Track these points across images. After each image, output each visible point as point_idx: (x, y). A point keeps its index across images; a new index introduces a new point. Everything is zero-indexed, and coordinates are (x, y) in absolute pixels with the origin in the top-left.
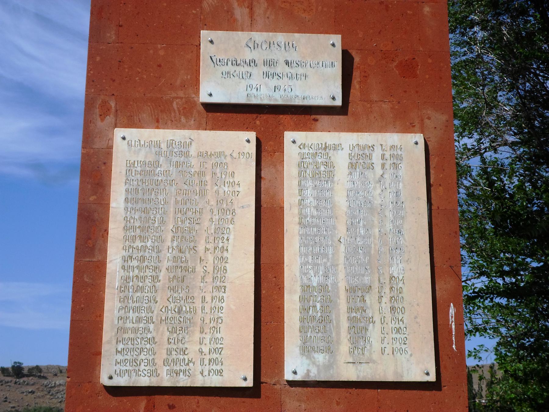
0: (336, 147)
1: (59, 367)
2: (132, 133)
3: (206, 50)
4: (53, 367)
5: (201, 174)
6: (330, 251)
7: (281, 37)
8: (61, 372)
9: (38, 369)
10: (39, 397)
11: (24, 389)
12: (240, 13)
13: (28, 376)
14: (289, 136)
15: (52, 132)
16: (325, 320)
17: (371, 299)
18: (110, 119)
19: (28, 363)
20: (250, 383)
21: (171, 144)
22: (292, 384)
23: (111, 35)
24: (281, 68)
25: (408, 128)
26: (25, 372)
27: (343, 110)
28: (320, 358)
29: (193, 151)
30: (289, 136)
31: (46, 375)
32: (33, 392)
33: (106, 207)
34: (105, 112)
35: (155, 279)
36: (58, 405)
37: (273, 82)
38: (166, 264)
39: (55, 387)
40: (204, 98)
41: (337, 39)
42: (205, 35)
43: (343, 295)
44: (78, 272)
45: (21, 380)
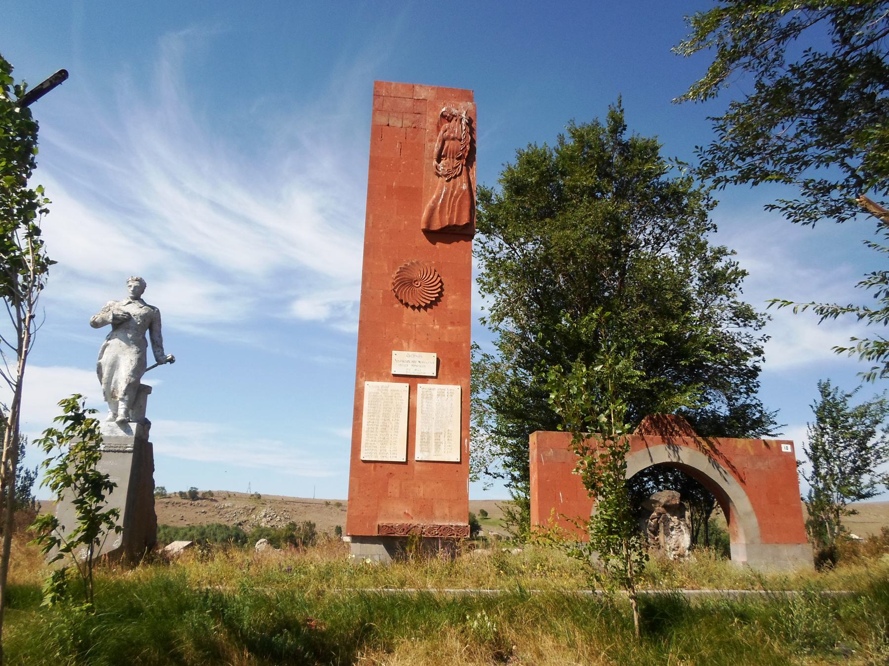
0: (433, 389)
1: (228, 492)
2: (370, 383)
3: (394, 357)
4: (223, 492)
5: (391, 396)
6: (661, 245)
7: (417, 354)
8: (229, 496)
9: (211, 493)
10: (210, 517)
11: (198, 510)
12: (405, 344)
13: (201, 499)
14: (419, 385)
15: (219, 297)
16: (428, 442)
17: (442, 436)
18: (364, 378)
19: (202, 488)
20: (405, 460)
21: (382, 387)
22: (417, 461)
23: (364, 351)
24: (418, 364)
25: (456, 384)
26: (200, 495)
27: (436, 377)
28: (426, 454)
29: (389, 389)
30: (419, 385)
31: (216, 498)
32: (205, 513)
33: (362, 406)
34: (362, 376)
35: (377, 428)
36: (226, 523)
37: (415, 368)
38: (380, 425)
39: (223, 508)
40: (393, 372)
41: (435, 355)
42: (394, 352)
43: (433, 435)
44: (354, 426)
45: (196, 502)
